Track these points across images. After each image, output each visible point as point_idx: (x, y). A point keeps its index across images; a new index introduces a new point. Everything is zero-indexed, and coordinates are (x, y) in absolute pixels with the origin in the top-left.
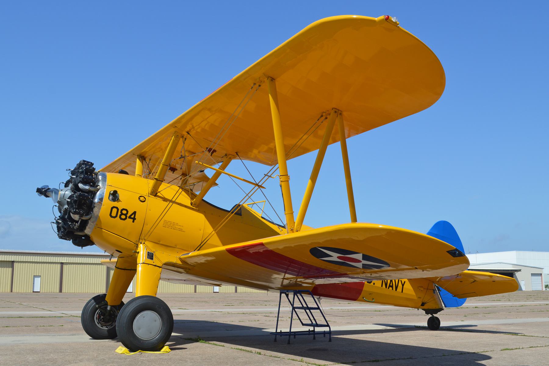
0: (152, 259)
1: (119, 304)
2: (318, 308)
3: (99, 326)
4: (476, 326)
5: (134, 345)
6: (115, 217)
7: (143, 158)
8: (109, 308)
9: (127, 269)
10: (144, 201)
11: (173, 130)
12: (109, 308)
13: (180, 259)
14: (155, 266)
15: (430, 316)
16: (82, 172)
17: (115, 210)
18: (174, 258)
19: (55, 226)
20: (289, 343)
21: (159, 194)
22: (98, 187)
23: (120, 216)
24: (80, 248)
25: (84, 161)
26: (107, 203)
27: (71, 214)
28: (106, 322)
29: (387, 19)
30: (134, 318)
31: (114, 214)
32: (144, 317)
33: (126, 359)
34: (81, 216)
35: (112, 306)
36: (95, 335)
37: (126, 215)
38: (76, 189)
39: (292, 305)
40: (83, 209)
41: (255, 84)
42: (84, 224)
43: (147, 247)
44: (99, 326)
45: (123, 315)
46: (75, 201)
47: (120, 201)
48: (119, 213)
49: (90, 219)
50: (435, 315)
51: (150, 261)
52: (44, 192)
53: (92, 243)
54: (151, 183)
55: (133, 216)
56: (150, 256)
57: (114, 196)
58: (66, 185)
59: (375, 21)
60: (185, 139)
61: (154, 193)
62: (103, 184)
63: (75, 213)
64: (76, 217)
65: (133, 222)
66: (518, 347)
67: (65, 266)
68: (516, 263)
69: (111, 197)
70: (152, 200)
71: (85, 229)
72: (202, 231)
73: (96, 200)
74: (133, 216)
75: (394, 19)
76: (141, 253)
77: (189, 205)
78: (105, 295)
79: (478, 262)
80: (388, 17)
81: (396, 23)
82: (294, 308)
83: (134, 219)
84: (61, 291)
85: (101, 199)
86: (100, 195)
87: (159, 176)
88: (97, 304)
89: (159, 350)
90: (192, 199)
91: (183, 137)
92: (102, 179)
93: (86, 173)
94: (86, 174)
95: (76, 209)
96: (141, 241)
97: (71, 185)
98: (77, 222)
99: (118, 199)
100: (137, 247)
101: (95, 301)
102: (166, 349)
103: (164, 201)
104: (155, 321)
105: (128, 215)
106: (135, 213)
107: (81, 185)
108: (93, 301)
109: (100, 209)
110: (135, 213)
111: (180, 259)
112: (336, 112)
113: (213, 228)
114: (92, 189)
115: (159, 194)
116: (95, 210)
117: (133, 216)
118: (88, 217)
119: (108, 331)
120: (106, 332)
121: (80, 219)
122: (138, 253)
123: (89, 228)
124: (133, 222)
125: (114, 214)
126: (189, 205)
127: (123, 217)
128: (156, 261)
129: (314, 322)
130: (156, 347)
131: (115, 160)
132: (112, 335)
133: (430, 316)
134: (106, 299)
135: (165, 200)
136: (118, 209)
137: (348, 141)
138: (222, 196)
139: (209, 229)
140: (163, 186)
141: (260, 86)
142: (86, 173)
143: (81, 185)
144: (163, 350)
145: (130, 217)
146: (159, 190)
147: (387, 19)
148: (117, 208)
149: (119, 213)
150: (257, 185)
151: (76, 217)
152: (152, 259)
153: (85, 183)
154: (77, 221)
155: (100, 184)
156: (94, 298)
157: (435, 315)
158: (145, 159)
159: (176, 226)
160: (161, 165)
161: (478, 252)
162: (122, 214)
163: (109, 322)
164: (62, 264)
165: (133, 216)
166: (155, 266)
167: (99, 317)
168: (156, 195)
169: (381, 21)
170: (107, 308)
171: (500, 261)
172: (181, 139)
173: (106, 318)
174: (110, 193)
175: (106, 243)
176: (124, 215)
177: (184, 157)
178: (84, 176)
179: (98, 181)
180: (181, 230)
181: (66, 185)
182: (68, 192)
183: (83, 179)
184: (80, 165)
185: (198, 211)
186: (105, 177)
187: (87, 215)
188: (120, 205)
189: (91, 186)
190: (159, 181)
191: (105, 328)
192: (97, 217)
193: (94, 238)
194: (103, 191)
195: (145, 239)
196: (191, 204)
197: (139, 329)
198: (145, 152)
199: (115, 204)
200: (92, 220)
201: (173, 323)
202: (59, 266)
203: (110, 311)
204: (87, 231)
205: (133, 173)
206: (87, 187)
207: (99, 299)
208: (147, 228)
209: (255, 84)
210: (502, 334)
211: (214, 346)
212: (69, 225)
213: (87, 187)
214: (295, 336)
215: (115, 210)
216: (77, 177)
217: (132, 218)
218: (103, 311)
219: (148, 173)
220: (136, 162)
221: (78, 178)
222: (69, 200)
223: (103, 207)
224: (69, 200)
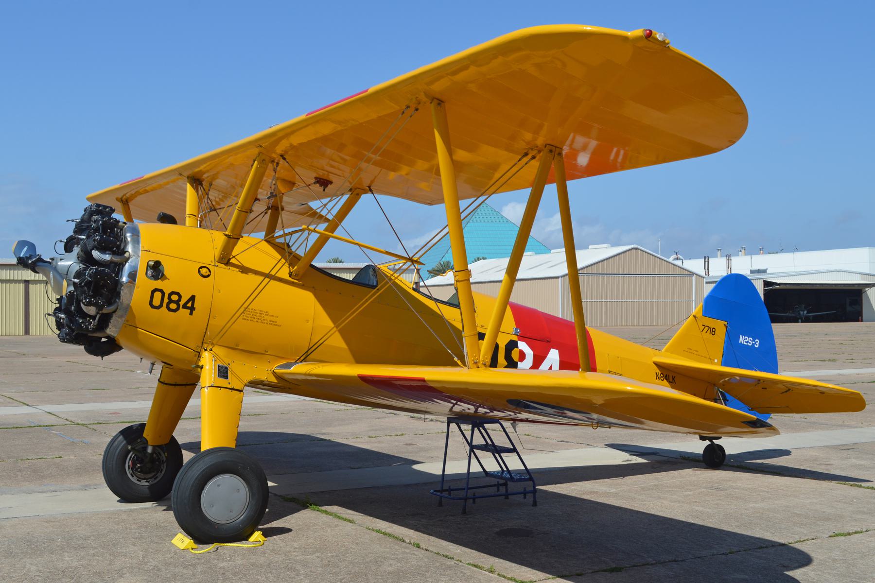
0: (226, 377)
1: (167, 441)
2: (514, 450)
3: (134, 480)
4: (787, 453)
5: (203, 532)
6: (158, 308)
7: (196, 181)
8: (150, 450)
9: (180, 384)
10: (209, 276)
11: (256, 151)
12: (150, 450)
13: (274, 373)
14: (232, 389)
15: (708, 443)
16: (97, 230)
17: (158, 295)
18: (265, 372)
19: (52, 320)
20: (464, 512)
21: (233, 261)
22: (127, 255)
23: (168, 304)
24: (100, 357)
25: (98, 205)
26: (145, 284)
27: (82, 305)
28: (145, 473)
29: (649, 35)
30: (203, 489)
31: (157, 301)
32: (219, 486)
33: (194, 566)
34: (99, 308)
35: (154, 447)
36: (127, 495)
37: (177, 302)
38: (86, 259)
39: (470, 444)
40: (101, 295)
41: (408, 107)
42: (105, 321)
43: (215, 357)
44: (134, 480)
45: (183, 481)
46: (88, 283)
47: (166, 278)
48: (166, 300)
49: (115, 312)
50: (716, 442)
51: (222, 382)
52: (30, 261)
53: (118, 348)
54: (219, 238)
55: (189, 305)
56: (223, 372)
57: (156, 270)
58: (68, 248)
59: (625, 39)
60: (278, 164)
61: (225, 259)
62: (134, 247)
63: (89, 304)
64: (91, 310)
65: (191, 314)
66: (859, 530)
67: (32, 287)
68: (868, 272)
69: (150, 272)
70: (221, 272)
71: (107, 326)
72: (311, 323)
73: (124, 279)
74: (190, 305)
75: (659, 36)
76: (207, 367)
77: (287, 277)
78: (142, 426)
79: (798, 269)
80: (651, 32)
81: (664, 42)
82: (472, 448)
83: (192, 309)
84: (27, 332)
85: (133, 276)
86: (131, 266)
87: (233, 231)
88: (129, 443)
89: (246, 538)
90: (291, 265)
91: (273, 161)
92: (132, 240)
93: (105, 232)
94: (101, 230)
95: (91, 297)
96: (205, 346)
97: (77, 250)
98: (94, 318)
99: (163, 274)
100: (199, 356)
101: (125, 438)
102: (257, 536)
103: (242, 272)
104: (238, 490)
105: (182, 303)
106: (193, 298)
107: (96, 254)
108: (121, 437)
109: (131, 294)
110: (193, 298)
111: (274, 373)
112: (551, 151)
113: (334, 323)
114: (116, 259)
115: (233, 261)
116: (124, 293)
117: (189, 305)
118: (112, 308)
119: (150, 487)
120: (147, 491)
121: (98, 313)
122: (202, 367)
123: (115, 326)
124: (191, 314)
125: (157, 301)
126: (287, 277)
127: (173, 306)
128: (233, 381)
129: (463, 216)
130: (241, 534)
131: (147, 176)
132: (158, 494)
133: (708, 443)
134: (145, 435)
135: (244, 270)
136: (163, 293)
137: (569, 183)
138: (342, 257)
139: (326, 322)
140: (240, 246)
141: (417, 110)
142: (105, 232)
143: (96, 254)
144: (252, 539)
145: (185, 306)
146: (234, 254)
147: (649, 35)
148: (161, 291)
149: (166, 300)
150: (410, 259)
151: (91, 310)
152: (226, 377)
153: (103, 249)
154: (92, 314)
155: (130, 248)
156: (122, 432)
157: (716, 442)
158: (201, 184)
159: (266, 317)
160: (236, 212)
161: (797, 250)
162: (171, 301)
163: (150, 473)
164: (27, 282)
165: (190, 305)
166: (232, 389)
167: (134, 465)
168: (228, 263)
169: (637, 39)
170: (145, 448)
171: (838, 269)
172: (270, 165)
173: (147, 465)
174: (148, 265)
175: (144, 349)
176: (175, 302)
177: (276, 196)
178: (102, 237)
179: (126, 243)
180: (273, 323)
181: (68, 248)
182: (70, 262)
183: (99, 243)
184: (89, 213)
185: (303, 287)
186: (136, 233)
187: (110, 303)
188: (167, 286)
189: (114, 253)
190: (233, 239)
191: (144, 483)
192: (128, 308)
193: (122, 342)
194: (137, 257)
195: (212, 344)
196: (290, 275)
197: (212, 506)
198: (202, 173)
199: (158, 284)
200: (119, 313)
201: (268, 492)
202: (22, 286)
203: (152, 454)
204: (111, 331)
205: (184, 224)
206: (107, 257)
207: (133, 434)
208: (217, 323)
209: (408, 107)
210: (833, 484)
211: (336, 521)
212: (80, 324)
213: (107, 257)
214: (474, 499)
215: (158, 295)
216: (88, 237)
217: (188, 308)
218: (139, 455)
219: (208, 215)
220: (185, 190)
221: (91, 241)
222: (77, 281)
223: (138, 293)
224: (77, 281)
